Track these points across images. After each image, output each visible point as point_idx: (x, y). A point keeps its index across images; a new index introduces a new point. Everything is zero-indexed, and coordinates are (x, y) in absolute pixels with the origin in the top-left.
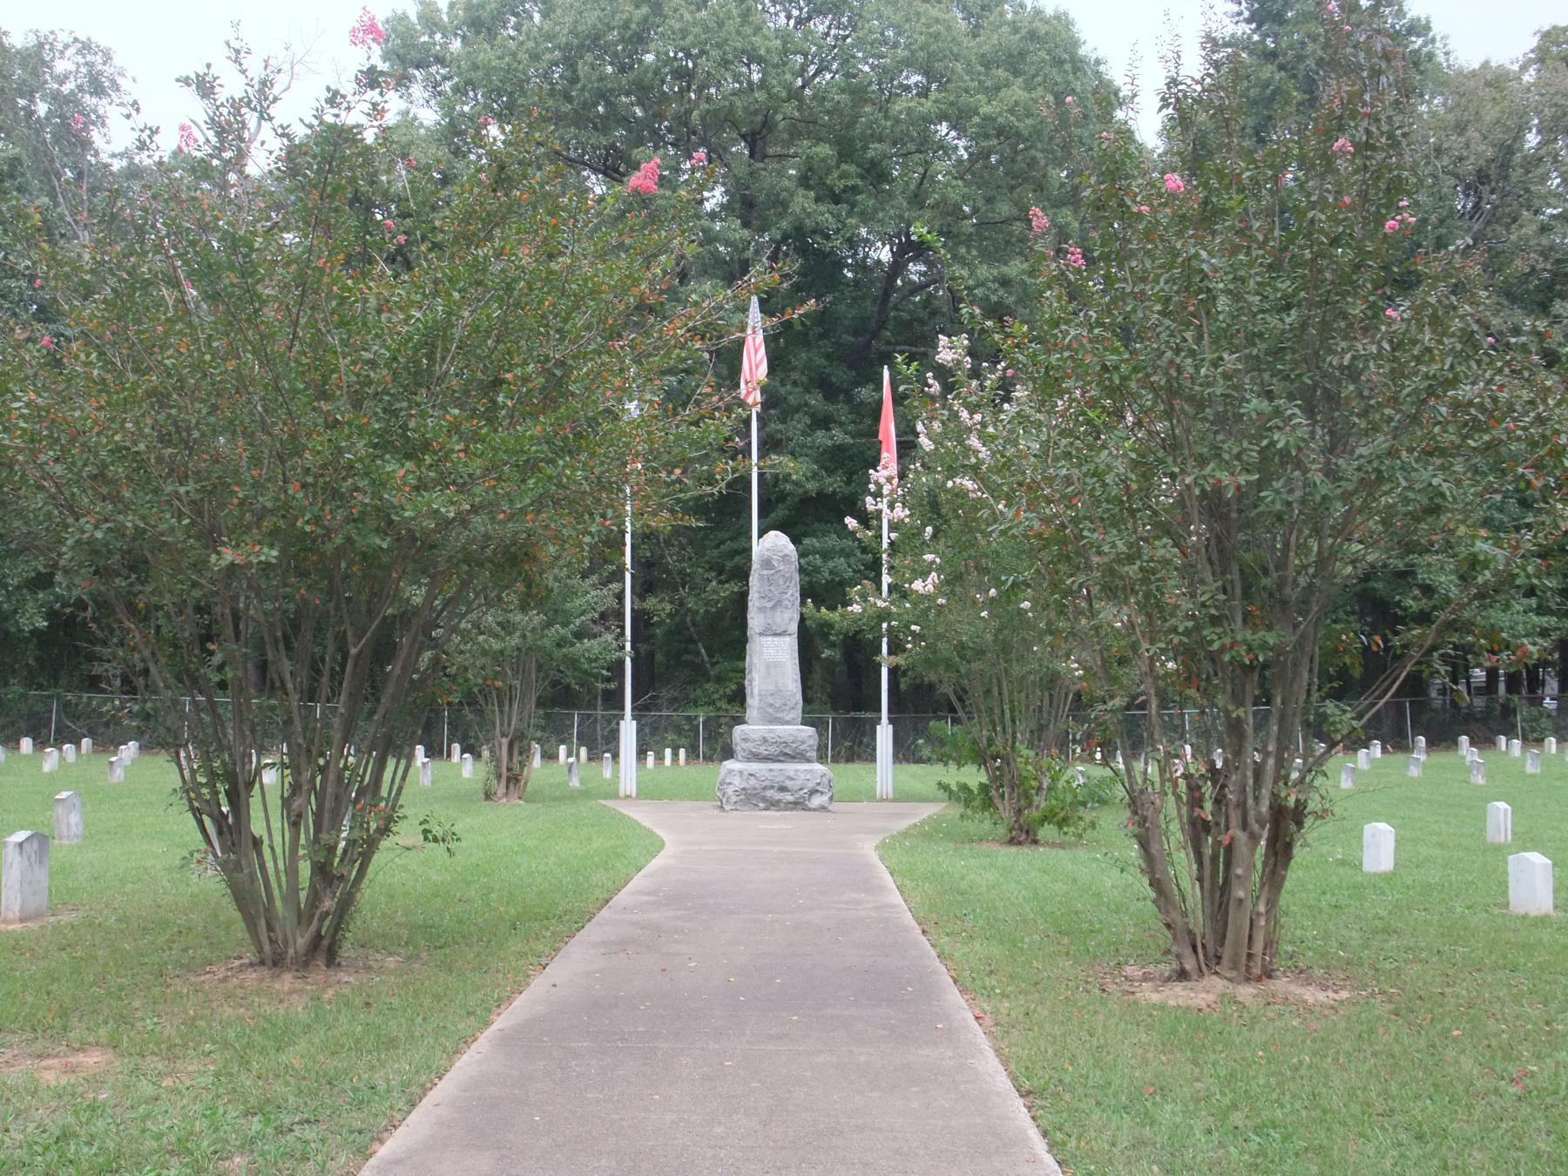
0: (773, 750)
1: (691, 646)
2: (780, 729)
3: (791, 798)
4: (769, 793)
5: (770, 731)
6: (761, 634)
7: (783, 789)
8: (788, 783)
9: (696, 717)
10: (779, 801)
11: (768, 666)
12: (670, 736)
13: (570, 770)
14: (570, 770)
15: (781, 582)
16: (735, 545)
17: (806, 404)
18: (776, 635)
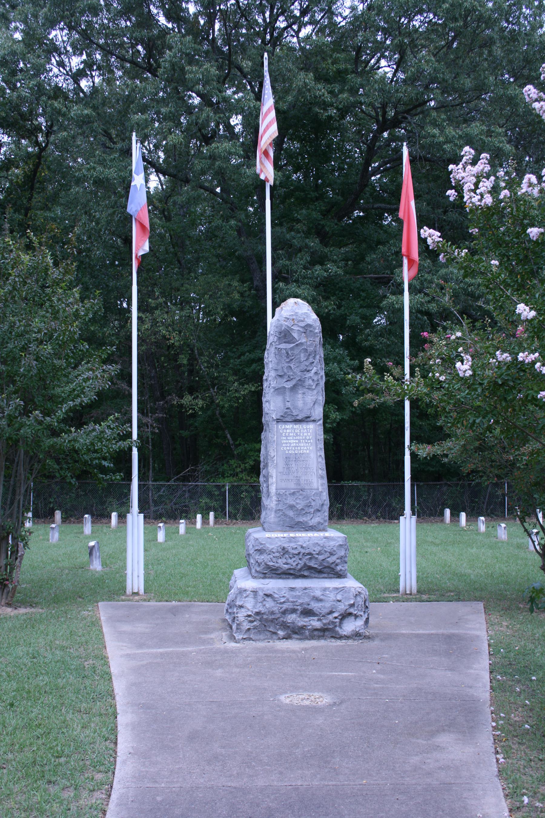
0: (294, 563)
1: (220, 433)
2: (303, 535)
3: (317, 624)
4: (291, 618)
5: (291, 540)
6: (278, 421)
7: (308, 613)
8: (315, 606)
9: (224, 486)
10: (303, 628)
11: (287, 459)
12: (204, 500)
13: (91, 554)
14: (91, 554)
15: (303, 357)
16: (252, 356)
17: (307, 246)
18: (297, 421)
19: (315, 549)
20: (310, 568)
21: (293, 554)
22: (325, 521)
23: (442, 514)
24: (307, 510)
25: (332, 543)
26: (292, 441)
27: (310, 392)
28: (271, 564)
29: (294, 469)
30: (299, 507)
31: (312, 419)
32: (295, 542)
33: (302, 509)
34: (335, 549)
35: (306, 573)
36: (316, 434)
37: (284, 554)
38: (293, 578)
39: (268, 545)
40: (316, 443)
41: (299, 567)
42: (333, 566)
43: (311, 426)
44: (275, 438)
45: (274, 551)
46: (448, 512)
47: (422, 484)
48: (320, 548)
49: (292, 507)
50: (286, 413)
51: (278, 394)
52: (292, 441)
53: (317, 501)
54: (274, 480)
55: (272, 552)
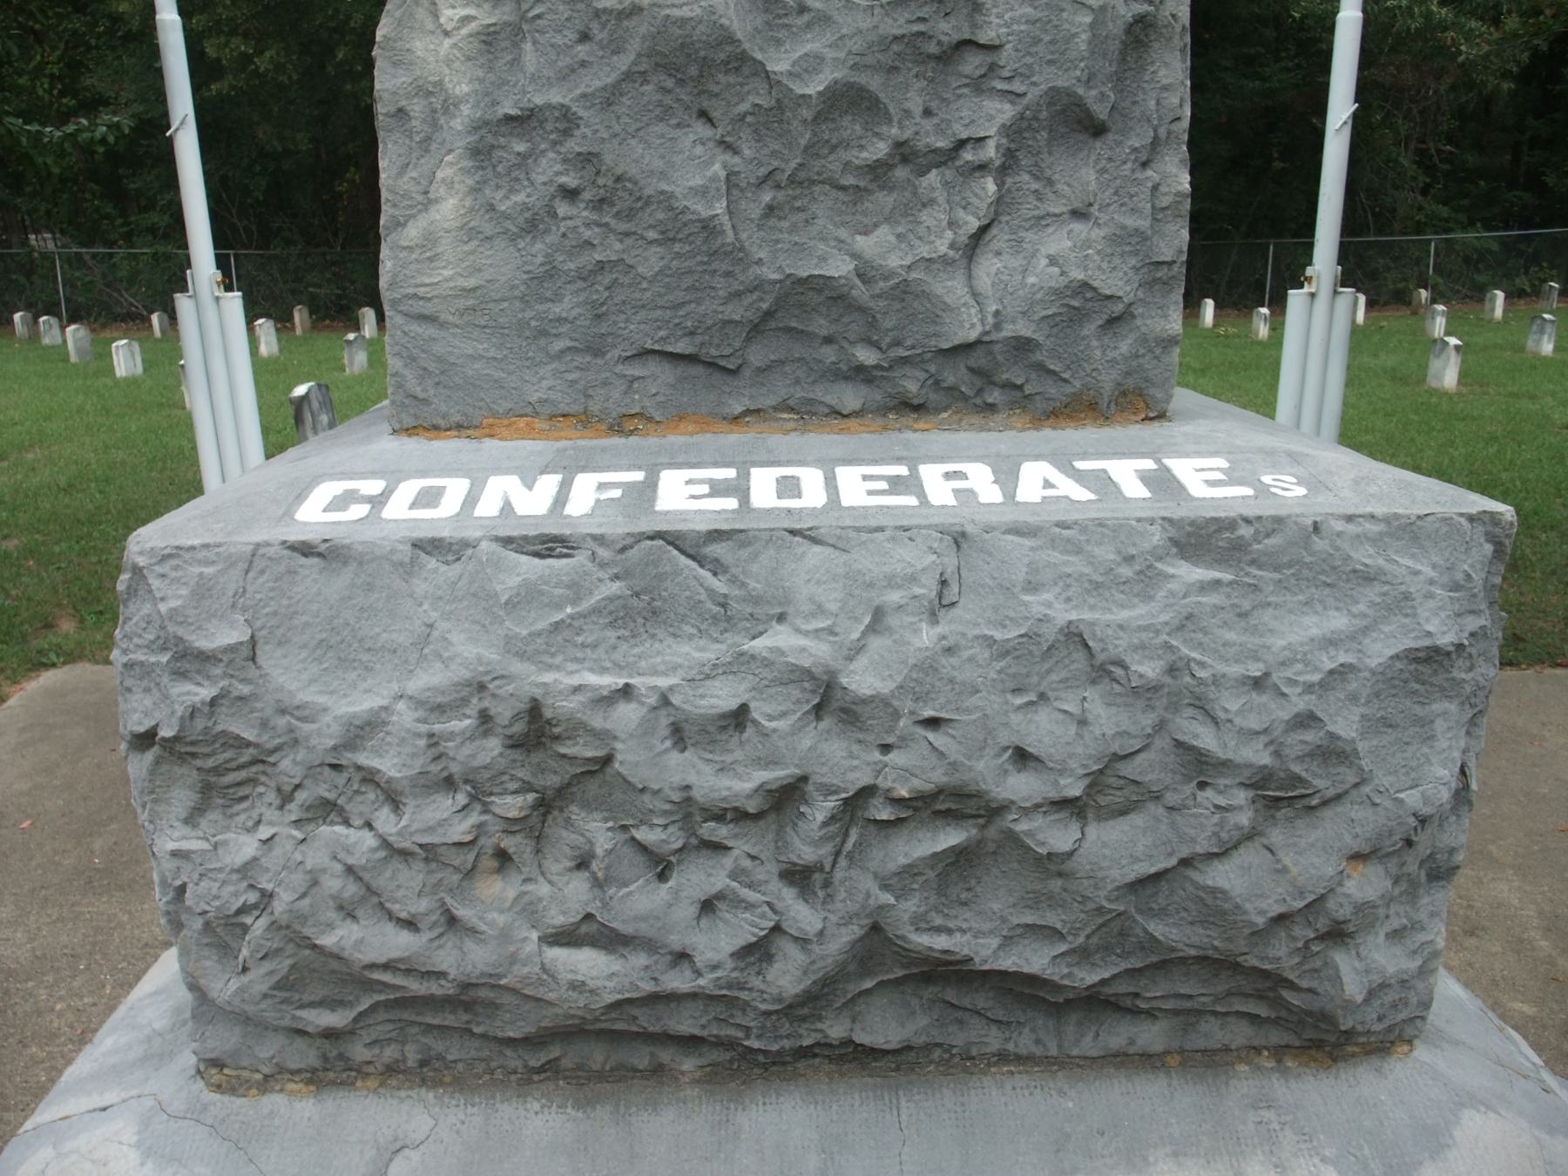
0: (700, 923)
5: (659, 575)
19: (1043, 730)
20: (944, 975)
21: (688, 809)
22: (1152, 275)
24: (911, 110)
25: (1301, 630)
28: (369, 941)
32: (723, 616)
33: (849, 100)
34: (1345, 724)
35: (883, 1027)
37: (547, 805)
38: (713, 1078)
39: (288, 675)
41: (787, 976)
42: (1280, 954)
45: (389, 765)
48: (1109, 720)
55: (342, 782)
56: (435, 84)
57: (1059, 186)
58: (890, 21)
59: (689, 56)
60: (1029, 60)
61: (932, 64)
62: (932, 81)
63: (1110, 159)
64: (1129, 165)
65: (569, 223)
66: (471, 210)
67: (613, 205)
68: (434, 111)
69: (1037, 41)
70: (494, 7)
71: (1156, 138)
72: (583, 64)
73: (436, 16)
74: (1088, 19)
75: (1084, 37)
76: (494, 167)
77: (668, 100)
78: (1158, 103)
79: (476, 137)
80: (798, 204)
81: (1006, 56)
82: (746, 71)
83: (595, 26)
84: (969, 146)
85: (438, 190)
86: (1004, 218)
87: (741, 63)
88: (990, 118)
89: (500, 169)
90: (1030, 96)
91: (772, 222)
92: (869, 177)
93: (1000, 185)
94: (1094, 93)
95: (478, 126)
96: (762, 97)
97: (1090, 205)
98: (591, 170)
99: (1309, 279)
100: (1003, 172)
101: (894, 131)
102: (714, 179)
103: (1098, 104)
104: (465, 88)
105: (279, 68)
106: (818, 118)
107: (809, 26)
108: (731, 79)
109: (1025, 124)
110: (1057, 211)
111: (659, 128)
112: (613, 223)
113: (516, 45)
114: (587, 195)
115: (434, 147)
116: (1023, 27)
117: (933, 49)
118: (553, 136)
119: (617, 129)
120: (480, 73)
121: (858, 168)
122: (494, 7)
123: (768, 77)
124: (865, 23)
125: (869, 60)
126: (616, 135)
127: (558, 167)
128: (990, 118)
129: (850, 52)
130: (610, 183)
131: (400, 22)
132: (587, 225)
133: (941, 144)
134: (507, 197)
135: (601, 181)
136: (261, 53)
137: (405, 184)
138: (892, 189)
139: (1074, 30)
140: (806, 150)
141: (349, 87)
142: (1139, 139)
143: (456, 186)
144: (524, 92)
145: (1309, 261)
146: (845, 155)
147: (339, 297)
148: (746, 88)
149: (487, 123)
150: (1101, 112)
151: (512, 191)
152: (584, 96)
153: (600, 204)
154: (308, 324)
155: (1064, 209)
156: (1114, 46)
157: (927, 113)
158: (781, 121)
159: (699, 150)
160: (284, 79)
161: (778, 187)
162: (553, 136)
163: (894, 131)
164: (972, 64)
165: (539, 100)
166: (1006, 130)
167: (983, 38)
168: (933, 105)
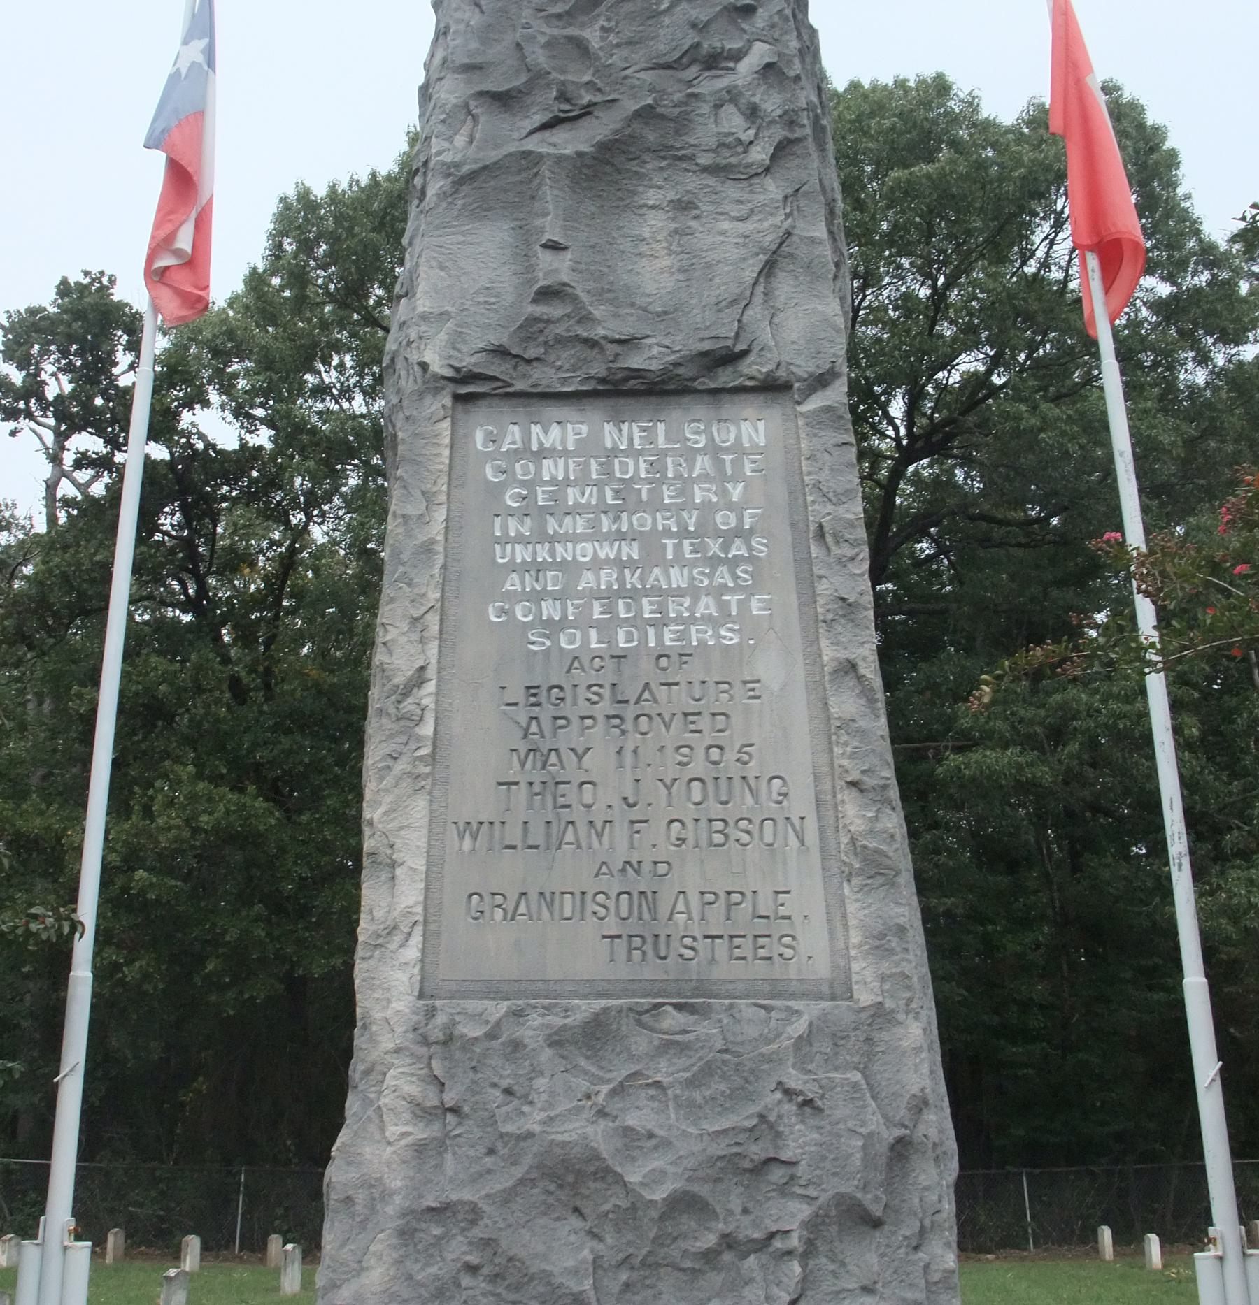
6: (469, 389)
11: (541, 701)
23: (1094, 1237)
24: (734, 1211)
26: (585, 551)
27: (732, 191)
29: (605, 798)
30: (653, 1177)
31: (754, 368)
36: (796, 491)
40: (803, 563)
43: (753, 428)
44: (436, 528)
46: (1106, 1234)
47: (1037, 1171)
49: (572, 1179)
50: (531, 328)
51: (481, 211)
52: (585, 551)
53: (839, 1109)
54: (410, 895)
56: (377, 1179)
57: (850, 1267)
58: (715, 1145)
59: (567, 1168)
60: (818, 1172)
61: (747, 1175)
62: (747, 1187)
63: (888, 1246)
64: (903, 1250)
65: (470, 1292)
66: (394, 1278)
67: (504, 1279)
68: (373, 1199)
69: (824, 1158)
70: (427, 1126)
71: (922, 1227)
72: (489, 1171)
73: (382, 1130)
74: (860, 1143)
75: (858, 1156)
76: (415, 1245)
77: (550, 1200)
78: (921, 1200)
79: (403, 1222)
80: (648, 1282)
81: (801, 1170)
82: (610, 1180)
83: (499, 1145)
84: (778, 1237)
85: (370, 1261)
86: (810, 1293)
87: (606, 1174)
88: (793, 1215)
89: (420, 1247)
90: (821, 1199)
91: (628, 1296)
92: (703, 1261)
93: (804, 1267)
94: (869, 1196)
95: (406, 1213)
96: (619, 1200)
97: (875, 1283)
98: (490, 1251)
99: (1213, 1241)
100: (809, 1251)
101: (721, 1226)
102: (584, 1261)
103: (873, 1202)
104: (399, 1183)
105: (146, 977)
106: (663, 1217)
107: (656, 1147)
108: (599, 1185)
109: (819, 1220)
110: (850, 1287)
111: (543, 1221)
112: (504, 1293)
113: (440, 1154)
114: (485, 1271)
115: (370, 1225)
116: (813, 1149)
117: (747, 1164)
118: (462, 1225)
119: (511, 1220)
120: (412, 1174)
121: (694, 1254)
122: (427, 1126)
123: (625, 1185)
124: (697, 1148)
125: (701, 1174)
126: (510, 1226)
127: (465, 1248)
128: (793, 1215)
129: (685, 1169)
130: (504, 1262)
131: (356, 1133)
132: (484, 1295)
133: (756, 1235)
134: (423, 1269)
135: (497, 1261)
136: (129, 962)
137: (345, 1254)
138: (721, 1270)
139: (850, 1151)
140: (653, 1241)
141: (213, 998)
142: (909, 1228)
143: (384, 1258)
144: (443, 1190)
145: (1209, 1221)
146: (684, 1245)
147: (162, 1220)
148: (609, 1193)
149: (413, 1212)
150: (877, 1210)
151: (427, 1265)
152: (488, 1195)
153: (495, 1278)
154: (121, 1251)
155: (856, 1286)
156: (883, 1161)
157: (745, 1211)
158: (635, 1219)
159: (573, 1238)
160: (148, 988)
161: (633, 1268)
162: (462, 1225)
163: (721, 1226)
164: (777, 1175)
165: (454, 1197)
166: (805, 1225)
167: (784, 1156)
168: (750, 1205)
